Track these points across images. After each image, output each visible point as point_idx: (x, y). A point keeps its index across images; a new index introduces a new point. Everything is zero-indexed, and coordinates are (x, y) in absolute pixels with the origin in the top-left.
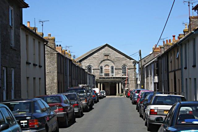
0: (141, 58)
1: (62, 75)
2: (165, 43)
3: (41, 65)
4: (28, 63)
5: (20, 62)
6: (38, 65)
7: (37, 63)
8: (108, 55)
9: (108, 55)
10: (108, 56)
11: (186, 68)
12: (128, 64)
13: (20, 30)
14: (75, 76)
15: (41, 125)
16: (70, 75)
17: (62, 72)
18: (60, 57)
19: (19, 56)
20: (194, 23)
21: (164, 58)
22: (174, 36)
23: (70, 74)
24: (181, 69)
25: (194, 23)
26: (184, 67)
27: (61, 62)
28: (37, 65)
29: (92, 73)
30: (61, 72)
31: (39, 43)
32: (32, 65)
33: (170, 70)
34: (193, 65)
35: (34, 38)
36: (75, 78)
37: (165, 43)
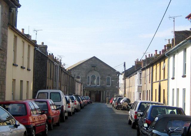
0: (125, 69)
1: (52, 80)
2: (151, 56)
3: (30, 69)
4: (14, 65)
5: (6, 63)
6: (26, 68)
7: (26, 66)
8: (95, 67)
9: (95, 67)
10: (95, 68)
11: (173, 78)
12: (112, 75)
13: (7, 29)
14: (64, 83)
15: (31, 128)
16: (60, 82)
17: (52, 78)
18: (50, 63)
19: (4, 56)
20: (177, 38)
21: (148, 69)
22: (156, 51)
23: (59, 80)
24: (168, 80)
25: (177, 38)
26: (171, 76)
27: (51, 71)
28: (25, 68)
29: (84, 76)
30: (51, 77)
31: (29, 46)
32: (19, 67)
33: (154, 80)
34: (172, 77)
35: (24, 40)
36: (64, 85)
37: (151, 56)
